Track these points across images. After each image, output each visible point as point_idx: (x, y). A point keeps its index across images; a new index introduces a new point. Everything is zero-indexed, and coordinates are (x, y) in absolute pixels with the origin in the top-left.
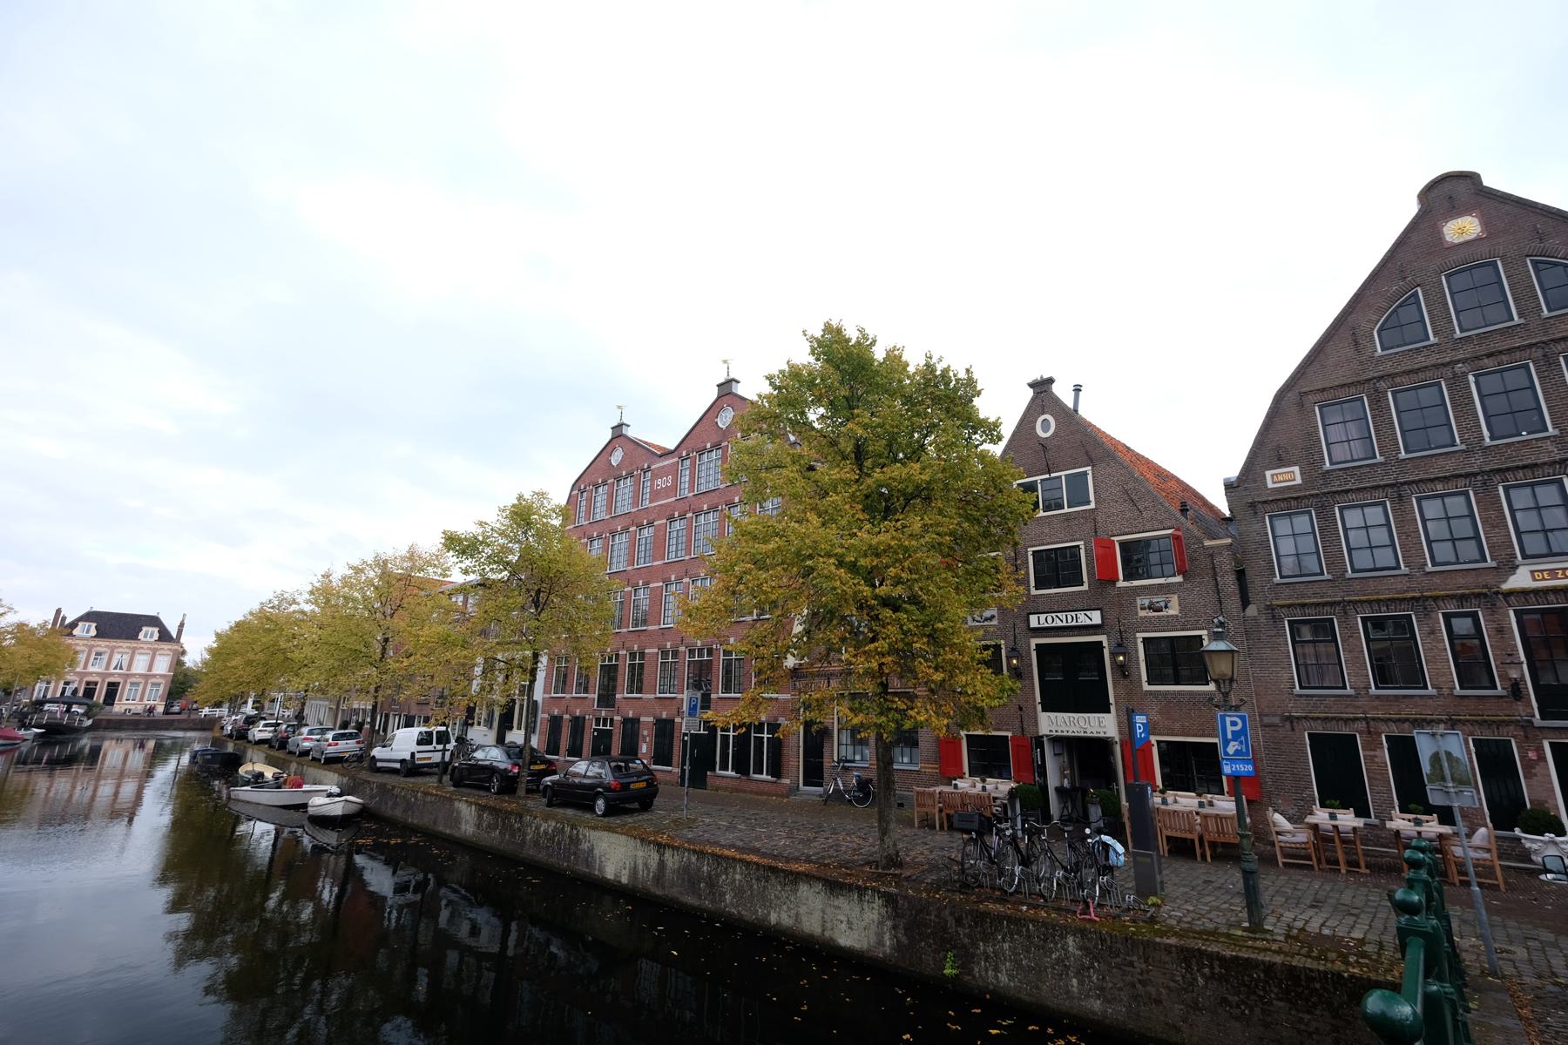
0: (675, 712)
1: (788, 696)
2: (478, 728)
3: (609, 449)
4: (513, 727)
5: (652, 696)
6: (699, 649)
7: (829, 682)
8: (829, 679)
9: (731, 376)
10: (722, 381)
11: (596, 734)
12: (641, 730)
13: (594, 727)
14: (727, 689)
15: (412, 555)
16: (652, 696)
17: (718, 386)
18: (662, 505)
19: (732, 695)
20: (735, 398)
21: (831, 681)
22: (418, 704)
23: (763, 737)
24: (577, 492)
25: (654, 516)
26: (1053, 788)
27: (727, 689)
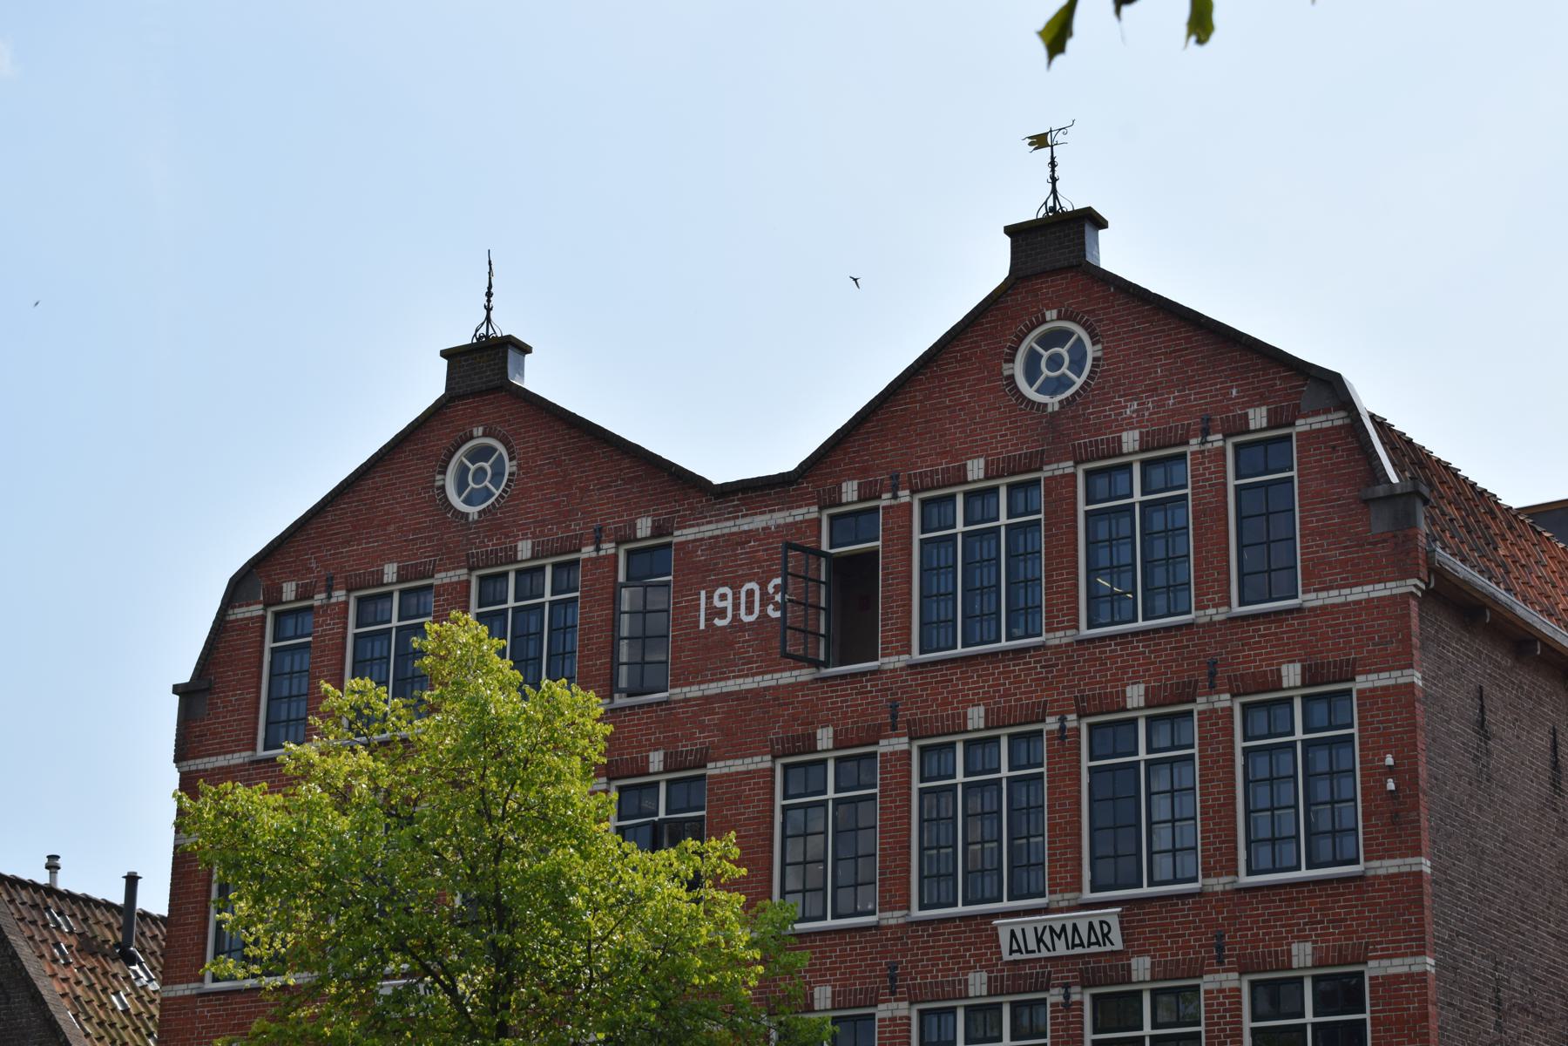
25: (702, 739)
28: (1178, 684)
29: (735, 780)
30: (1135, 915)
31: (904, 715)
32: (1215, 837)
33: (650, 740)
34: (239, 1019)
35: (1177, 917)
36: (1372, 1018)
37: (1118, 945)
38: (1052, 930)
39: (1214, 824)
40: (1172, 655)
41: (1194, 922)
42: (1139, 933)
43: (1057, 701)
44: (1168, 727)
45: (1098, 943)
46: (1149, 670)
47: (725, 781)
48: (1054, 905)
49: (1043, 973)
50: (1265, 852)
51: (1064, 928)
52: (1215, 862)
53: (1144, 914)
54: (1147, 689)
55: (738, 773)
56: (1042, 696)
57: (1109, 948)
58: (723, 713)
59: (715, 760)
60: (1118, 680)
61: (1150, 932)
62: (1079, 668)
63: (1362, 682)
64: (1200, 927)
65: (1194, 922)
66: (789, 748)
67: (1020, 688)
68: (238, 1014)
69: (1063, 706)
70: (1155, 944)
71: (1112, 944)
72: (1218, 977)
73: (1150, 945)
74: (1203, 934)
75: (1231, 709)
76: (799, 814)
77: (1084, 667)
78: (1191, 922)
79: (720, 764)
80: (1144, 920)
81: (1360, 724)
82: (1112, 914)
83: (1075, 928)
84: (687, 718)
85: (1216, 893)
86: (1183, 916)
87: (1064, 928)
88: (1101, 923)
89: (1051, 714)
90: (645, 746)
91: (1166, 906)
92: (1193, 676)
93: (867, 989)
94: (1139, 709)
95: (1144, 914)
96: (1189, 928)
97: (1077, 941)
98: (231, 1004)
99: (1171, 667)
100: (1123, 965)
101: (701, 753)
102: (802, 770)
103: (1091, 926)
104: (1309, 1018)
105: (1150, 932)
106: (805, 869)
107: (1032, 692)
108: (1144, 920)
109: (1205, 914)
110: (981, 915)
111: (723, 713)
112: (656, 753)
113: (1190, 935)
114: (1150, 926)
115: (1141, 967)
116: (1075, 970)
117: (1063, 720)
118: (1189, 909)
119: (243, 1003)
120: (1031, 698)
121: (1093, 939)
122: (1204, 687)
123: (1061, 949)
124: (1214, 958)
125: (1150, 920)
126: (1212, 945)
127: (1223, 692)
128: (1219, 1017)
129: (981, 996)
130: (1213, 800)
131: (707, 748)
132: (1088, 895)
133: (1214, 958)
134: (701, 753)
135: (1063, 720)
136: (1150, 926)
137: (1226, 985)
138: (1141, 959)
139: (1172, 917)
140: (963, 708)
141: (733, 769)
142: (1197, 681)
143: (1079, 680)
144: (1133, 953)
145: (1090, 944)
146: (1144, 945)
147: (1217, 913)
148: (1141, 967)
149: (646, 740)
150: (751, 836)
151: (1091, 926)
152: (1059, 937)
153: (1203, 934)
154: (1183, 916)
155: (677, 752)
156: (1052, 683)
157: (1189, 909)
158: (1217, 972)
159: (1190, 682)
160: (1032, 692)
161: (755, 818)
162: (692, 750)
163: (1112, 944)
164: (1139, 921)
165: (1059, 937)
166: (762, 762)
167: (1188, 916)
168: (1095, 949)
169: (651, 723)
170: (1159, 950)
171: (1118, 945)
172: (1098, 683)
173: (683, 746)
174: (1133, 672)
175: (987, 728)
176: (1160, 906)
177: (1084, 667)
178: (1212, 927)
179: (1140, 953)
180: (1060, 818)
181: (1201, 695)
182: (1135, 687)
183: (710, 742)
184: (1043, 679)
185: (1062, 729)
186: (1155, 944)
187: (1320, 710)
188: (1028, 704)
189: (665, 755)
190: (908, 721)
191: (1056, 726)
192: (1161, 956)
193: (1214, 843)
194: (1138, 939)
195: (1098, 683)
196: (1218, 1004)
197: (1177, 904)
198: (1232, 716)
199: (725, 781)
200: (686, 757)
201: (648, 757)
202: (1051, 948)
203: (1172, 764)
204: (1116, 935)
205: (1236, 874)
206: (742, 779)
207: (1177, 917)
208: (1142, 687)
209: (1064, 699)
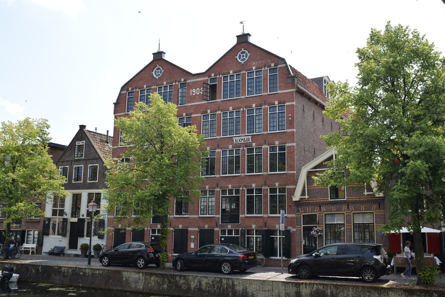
0: (214, 225)
1: (294, 215)
2: (54, 236)
3: (152, 67)
4: (49, 234)
5: (196, 216)
6: (229, 190)
7: (320, 208)
8: (320, 206)
9: (161, 50)
10: (156, 52)
11: (153, 238)
12: (189, 235)
13: (220, 235)
14: (250, 211)
15: (319, 81)
16: (196, 216)
17: (237, 36)
18: (196, 105)
19: (254, 215)
20: (250, 46)
21: (322, 207)
22: (27, 222)
23: (256, 235)
24: (125, 92)
25: (191, 111)
26: (80, 245)
27: (250, 211)
31: (220, 108)
50: (272, 128)
63: (287, 104)
82: (250, 137)
104: (278, 152)
132: (246, 134)
148: (254, 144)
166: (200, 115)
179: (254, 142)
185: (243, 110)
204: (250, 140)
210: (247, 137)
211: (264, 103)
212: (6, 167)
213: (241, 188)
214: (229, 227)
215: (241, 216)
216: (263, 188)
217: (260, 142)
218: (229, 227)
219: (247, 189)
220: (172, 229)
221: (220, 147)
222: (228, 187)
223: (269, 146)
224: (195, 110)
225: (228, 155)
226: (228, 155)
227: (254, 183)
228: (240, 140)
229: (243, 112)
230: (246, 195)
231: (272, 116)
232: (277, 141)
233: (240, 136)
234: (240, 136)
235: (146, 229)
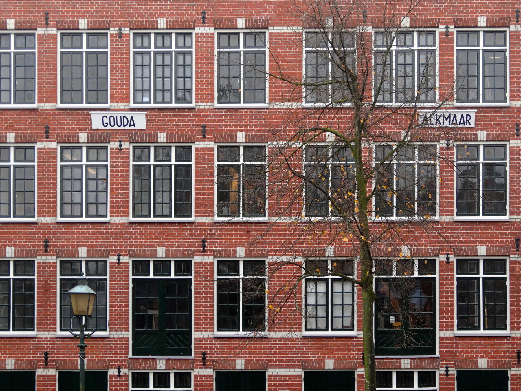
25: (265, 16)
28: (501, 19)
29: (284, 36)
30: (229, 115)
31: (370, 16)
32: (517, 84)
33: (237, 12)
34: (10, 123)
35: (499, 116)
36: (38, 165)
37: (473, 125)
38: (444, 116)
39: (517, 79)
40: (499, 6)
41: (506, 118)
42: (481, 121)
43: (444, 19)
44: (140, 38)
45: (464, 124)
46: (488, 11)
47: (278, 36)
48: (113, 108)
49: (507, 133)
50: (159, 95)
51: (449, 116)
52: (516, 95)
53: (484, 113)
54: (487, 19)
55: (285, 33)
56: (437, 16)
57: (468, 126)
58: (276, 4)
59: (273, 26)
60: (474, 14)
61: (486, 121)
62: (455, 6)
63: (273, 29)
64: (509, 121)
65: (506, 118)
66: (436, 23)
67: (427, 11)
68: (9, 120)
69: (447, 22)
70: (488, 126)
71: (470, 124)
72: (517, 141)
73: (486, 126)
74: (510, 124)
75: (56, 35)
76: (226, 56)
77: (458, 6)
78: (505, 118)
79: (275, 28)
80: (484, 116)
81: (38, 48)
82: (473, 113)
83: (455, 117)
84: (257, 4)
85: (517, 108)
86: (501, 116)
87: (449, 116)
88: (467, 115)
89: (442, 25)
90: (235, 15)
91: (494, 111)
92: (509, 16)
93: (184, 135)
94: (84, 29)
95: (484, 113)
96: (504, 121)
97: (132, 124)
98: (4, 115)
99: (499, 11)
100: (474, 134)
101: (265, 22)
102: (70, 37)
103: (462, 116)
104: (173, 162)
105: (486, 121)
106: (494, 79)
107: (432, 14)
108: (484, 116)
109: (511, 116)
110: (237, 108)
111: (276, 4)
112: (241, 19)
113: (504, 124)
114: (486, 118)
115: (482, 135)
116: (211, 135)
117: (447, 27)
118: (504, 113)
119: (11, 115)
120: (432, 16)
121: (462, 122)
122: (514, 21)
123: (446, 123)
124: (515, 134)
125: (486, 116)
126: (514, 129)
127: (369, 26)
128: (516, 158)
129: (483, 141)
130: (516, 69)
131: (269, 20)
132: (132, 105)
133: (515, 134)
134: (265, 22)
135: (447, 27)
136: (486, 118)
137: (52, 147)
138: (482, 132)
139: (496, 116)
140: (5, 19)
141: (282, 31)
142: (510, 18)
143: (456, 11)
144: (478, 129)
145: (460, 124)
146: (483, 126)
147: (517, 116)
148: (482, 135)
149: (235, 12)
150: (292, 62)
151: (462, 116)
152: (447, 120)
153: (510, 124)
154: (501, 116)
155: (252, 20)
156: (442, 11)
157: (504, 113)
158: (516, 139)
159: (507, 18)
160: (432, 14)
161: (294, 54)
162: (260, 20)
163: (470, 124)
164: (481, 116)
165: (447, 120)
166: (298, 29)
167: (503, 116)
168: (461, 126)
169: (238, 5)
170: (490, 129)
171: (473, 125)
172: (464, 13)
173: (255, 17)
174: (481, 11)
175: (167, 29)
176: (491, 111)
177: (458, 6)
178: (514, 121)
179: (482, 129)
180: (445, 69)
181: (512, 24)
182: (482, 17)
183: (270, 18)
184: (438, 8)
185: (447, 31)
186: (488, 126)
187: (21, 40)
188: (431, 19)
189: (246, 21)
190: (372, 19)
191: (445, 30)
192: (491, 131)
193: (516, 87)
194: (481, 124)
195: (464, 13)
196: (516, 152)
197: (499, 111)
198: (57, 38)
199: (278, 36)
200: (257, 23)
201: (236, 20)
202: (442, 123)
203: (468, 52)
204: (473, 121)
205: (57, 103)
206: (287, 36)
207: (499, 116)
208: (485, 18)
209: (448, 19)
210: (465, 112)
211: (514, 17)
212: (353, 132)
213: (113, 259)
214: (161, 365)
215: (439, 334)
216: (197, 259)
217: (502, 128)
218: (161, 365)
219: (133, 261)
220: (52, 372)
221: (208, 134)
222: (154, 254)
223: (60, 145)
224: (279, 14)
225: (12, 162)
226: (12, 162)
227: (482, 244)
228: (441, 120)
229: (447, 35)
230: (131, 277)
231: (139, 58)
232: (164, 131)
233: (108, 109)
234: (108, 109)
235: (112, 372)
